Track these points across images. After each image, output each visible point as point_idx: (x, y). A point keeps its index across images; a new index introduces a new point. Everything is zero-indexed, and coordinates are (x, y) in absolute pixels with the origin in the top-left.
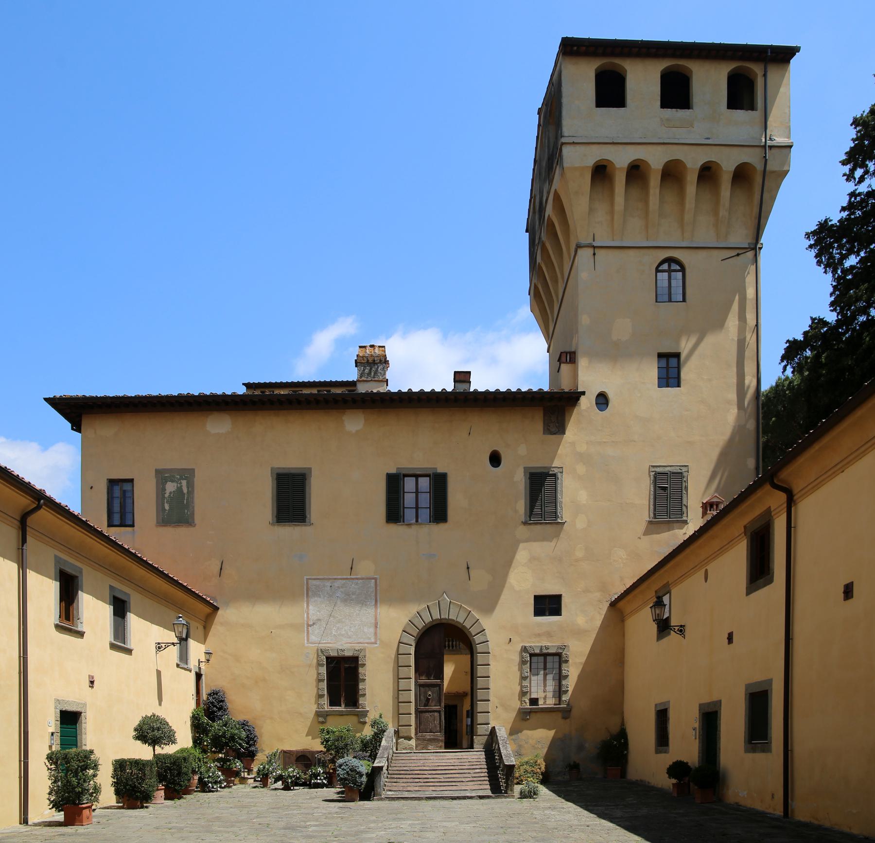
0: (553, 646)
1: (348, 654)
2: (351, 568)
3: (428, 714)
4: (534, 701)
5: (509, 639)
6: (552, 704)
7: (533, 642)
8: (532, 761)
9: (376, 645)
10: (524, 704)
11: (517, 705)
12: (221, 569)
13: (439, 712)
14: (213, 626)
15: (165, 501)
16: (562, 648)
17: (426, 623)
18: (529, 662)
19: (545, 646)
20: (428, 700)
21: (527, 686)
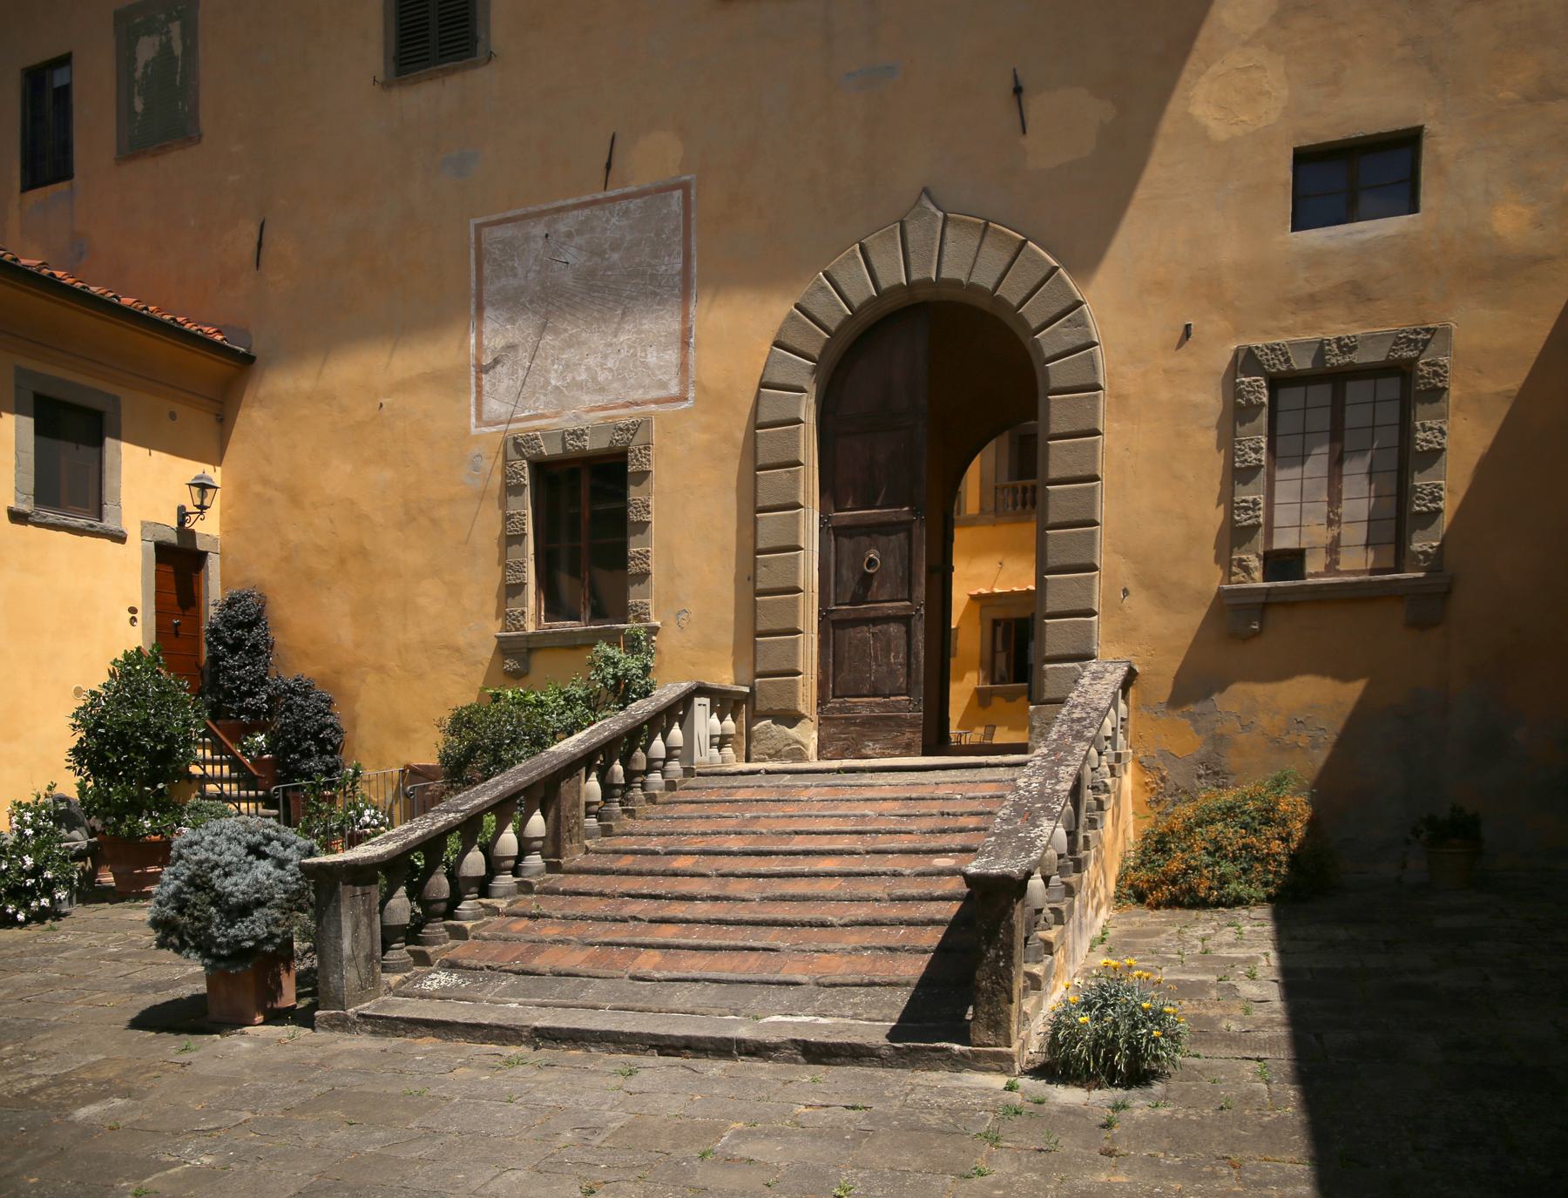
0: (1373, 337)
1: (591, 444)
2: (608, 166)
3: (865, 628)
4: (1284, 563)
5: (1181, 330)
6: (1363, 572)
7: (1287, 331)
8: (1250, 806)
9: (685, 405)
10: (1241, 576)
11: (1211, 579)
12: (260, 245)
13: (905, 620)
14: (240, 412)
15: (136, 89)
16: (1416, 341)
17: (856, 305)
18: (1265, 411)
19: (1339, 340)
20: (866, 580)
21: (1255, 503)
